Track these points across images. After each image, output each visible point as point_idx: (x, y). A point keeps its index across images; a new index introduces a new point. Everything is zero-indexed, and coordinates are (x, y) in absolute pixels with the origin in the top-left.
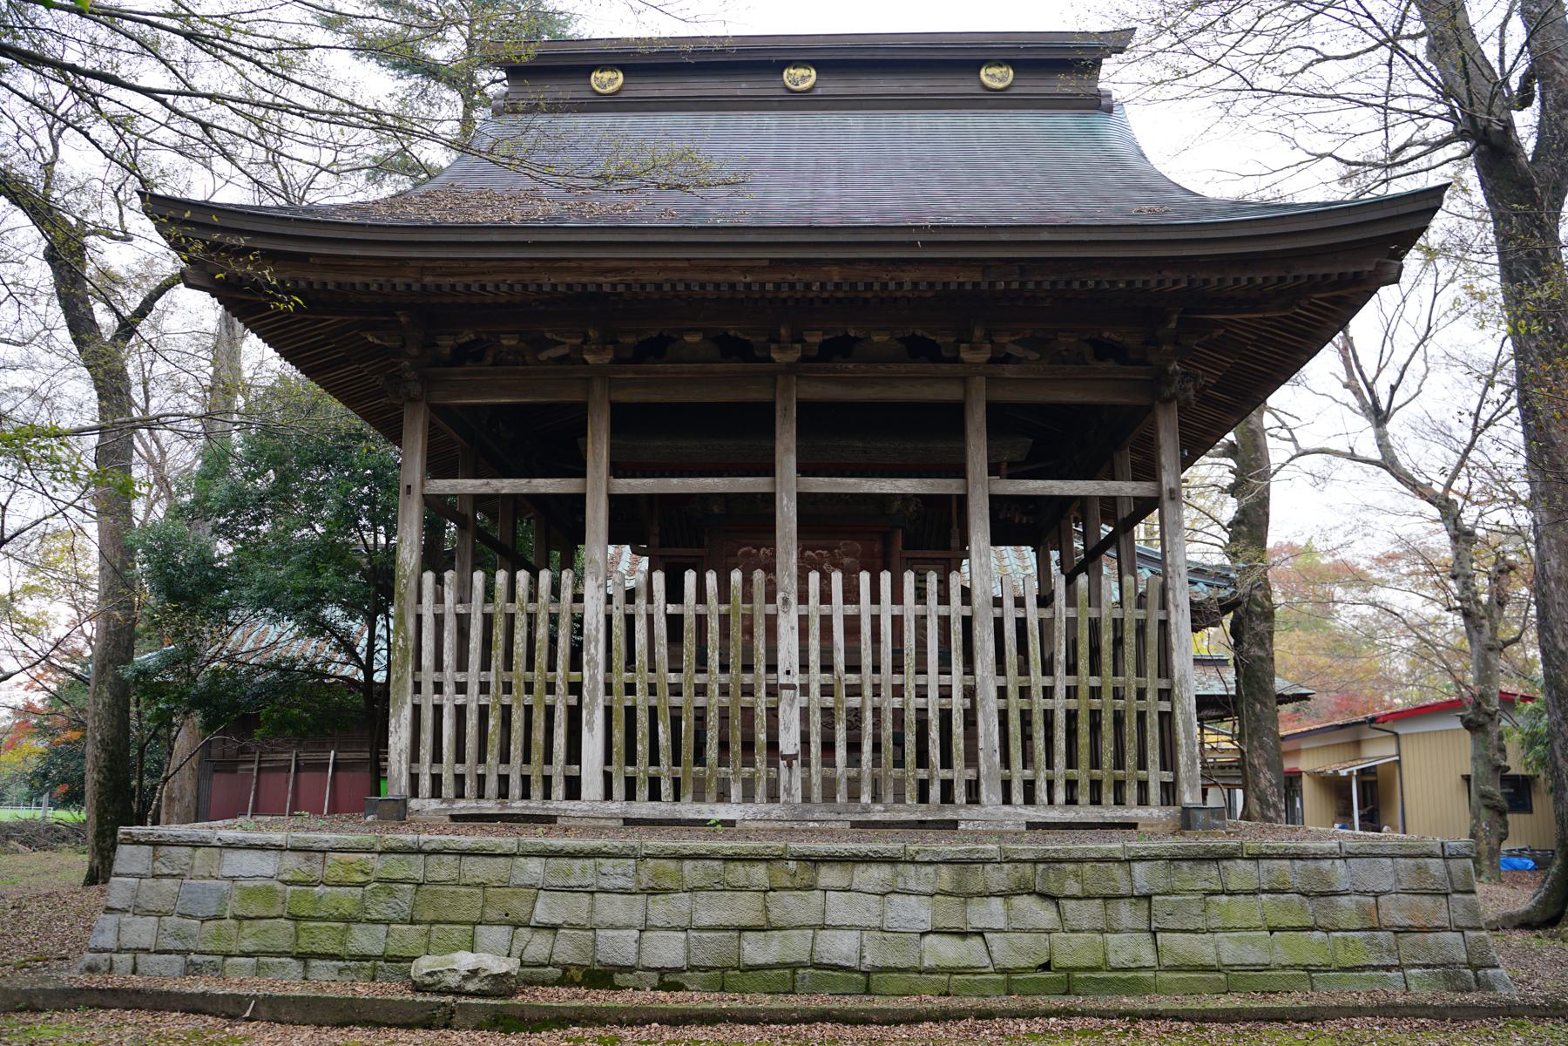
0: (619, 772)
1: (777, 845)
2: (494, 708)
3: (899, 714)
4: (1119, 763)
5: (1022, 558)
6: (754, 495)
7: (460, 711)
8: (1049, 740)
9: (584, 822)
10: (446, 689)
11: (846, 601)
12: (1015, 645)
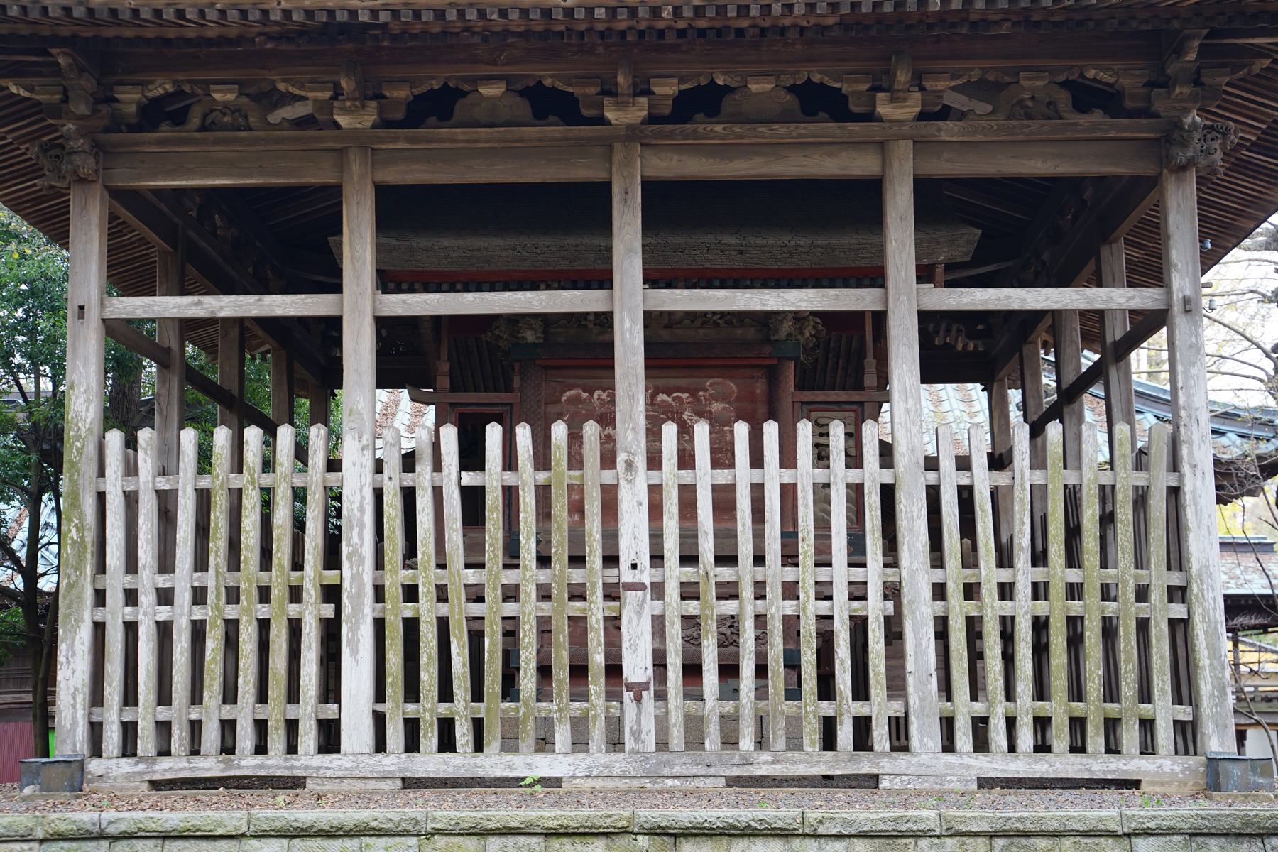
0: (396, 712)
1: (620, 814)
2: (214, 625)
3: (791, 625)
4: (1111, 693)
5: (968, 401)
6: (585, 315)
7: (164, 631)
8: (1008, 658)
9: (345, 785)
10: (142, 599)
11: (715, 464)
12: (959, 521)
